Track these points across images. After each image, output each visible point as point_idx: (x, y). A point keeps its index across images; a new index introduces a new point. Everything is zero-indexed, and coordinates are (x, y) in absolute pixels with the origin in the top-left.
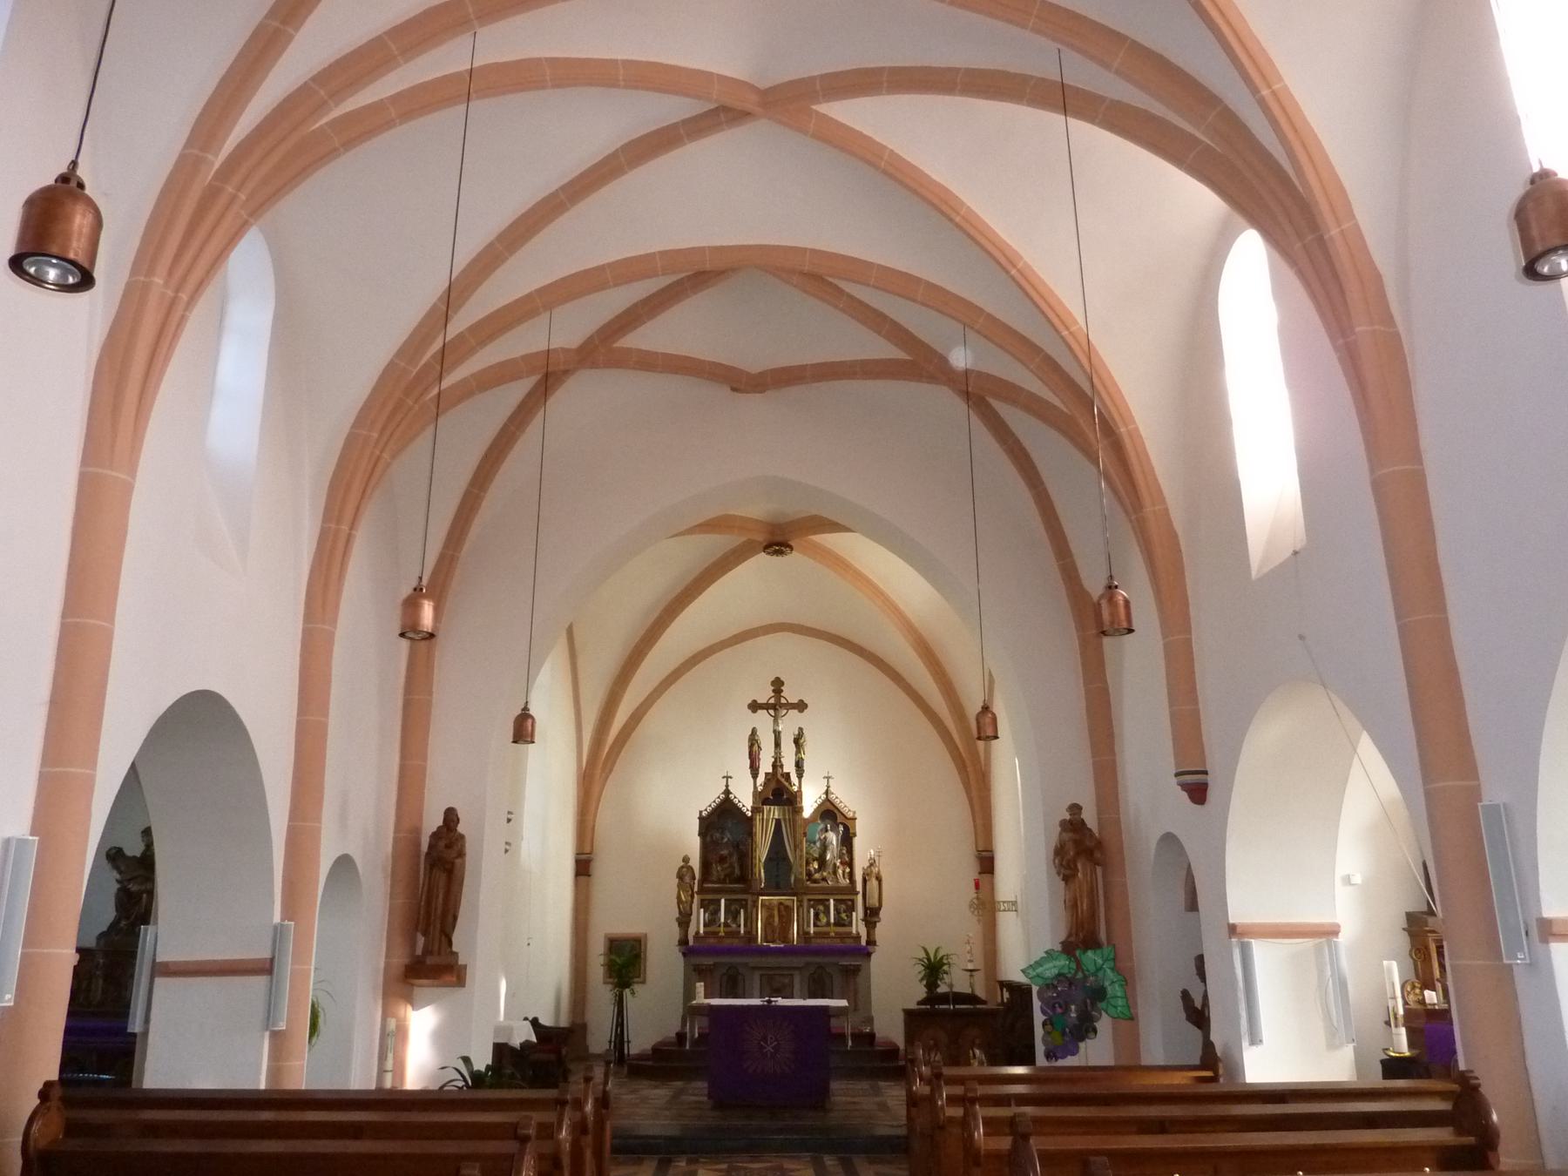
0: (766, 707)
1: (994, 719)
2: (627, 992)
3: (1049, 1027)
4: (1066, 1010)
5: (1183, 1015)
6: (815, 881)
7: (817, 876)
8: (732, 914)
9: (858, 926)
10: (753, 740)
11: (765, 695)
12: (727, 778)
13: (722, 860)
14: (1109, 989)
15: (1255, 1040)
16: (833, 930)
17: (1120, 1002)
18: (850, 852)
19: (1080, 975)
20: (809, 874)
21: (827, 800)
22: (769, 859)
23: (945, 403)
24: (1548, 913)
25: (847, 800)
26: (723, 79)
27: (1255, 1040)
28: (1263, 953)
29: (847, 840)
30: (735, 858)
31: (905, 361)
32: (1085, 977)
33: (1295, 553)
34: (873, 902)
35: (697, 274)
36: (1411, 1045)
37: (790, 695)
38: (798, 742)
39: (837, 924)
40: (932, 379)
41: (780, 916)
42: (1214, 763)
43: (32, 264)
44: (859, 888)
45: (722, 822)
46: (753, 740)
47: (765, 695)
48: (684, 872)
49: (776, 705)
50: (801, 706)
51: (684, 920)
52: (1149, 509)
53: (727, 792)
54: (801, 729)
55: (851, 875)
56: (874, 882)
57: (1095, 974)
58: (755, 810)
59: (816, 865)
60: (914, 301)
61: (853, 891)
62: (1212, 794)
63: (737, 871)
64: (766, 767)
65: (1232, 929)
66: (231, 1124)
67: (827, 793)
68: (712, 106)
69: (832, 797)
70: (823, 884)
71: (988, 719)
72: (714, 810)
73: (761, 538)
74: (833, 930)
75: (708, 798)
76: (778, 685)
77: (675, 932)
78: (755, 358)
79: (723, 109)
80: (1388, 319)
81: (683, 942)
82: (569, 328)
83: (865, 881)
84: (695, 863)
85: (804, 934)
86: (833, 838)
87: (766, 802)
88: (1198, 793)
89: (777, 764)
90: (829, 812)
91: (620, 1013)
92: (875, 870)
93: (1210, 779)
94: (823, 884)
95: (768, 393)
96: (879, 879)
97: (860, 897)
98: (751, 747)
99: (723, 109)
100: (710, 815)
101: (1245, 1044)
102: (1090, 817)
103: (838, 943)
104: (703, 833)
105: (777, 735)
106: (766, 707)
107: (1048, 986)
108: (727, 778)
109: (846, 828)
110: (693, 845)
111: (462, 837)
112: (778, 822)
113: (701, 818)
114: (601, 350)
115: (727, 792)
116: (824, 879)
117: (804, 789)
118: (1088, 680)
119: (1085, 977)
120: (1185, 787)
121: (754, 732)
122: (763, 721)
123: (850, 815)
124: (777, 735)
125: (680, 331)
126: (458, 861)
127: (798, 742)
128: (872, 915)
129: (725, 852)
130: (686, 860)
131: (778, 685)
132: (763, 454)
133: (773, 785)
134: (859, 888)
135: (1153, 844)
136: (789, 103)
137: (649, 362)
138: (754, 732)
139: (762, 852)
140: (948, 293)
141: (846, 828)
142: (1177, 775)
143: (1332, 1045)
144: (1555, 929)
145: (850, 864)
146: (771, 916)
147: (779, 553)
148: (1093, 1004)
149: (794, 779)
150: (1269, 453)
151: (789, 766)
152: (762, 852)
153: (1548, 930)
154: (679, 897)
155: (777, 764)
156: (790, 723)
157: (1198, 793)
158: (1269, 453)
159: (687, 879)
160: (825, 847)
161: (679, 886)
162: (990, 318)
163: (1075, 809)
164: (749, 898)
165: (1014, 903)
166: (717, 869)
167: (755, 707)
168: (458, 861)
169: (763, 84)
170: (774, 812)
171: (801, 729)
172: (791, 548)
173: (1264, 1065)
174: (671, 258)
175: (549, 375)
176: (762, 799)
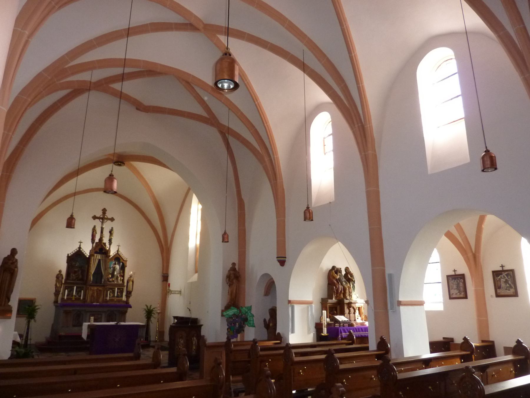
0: (99, 218)
1: (228, 236)
2: (32, 321)
3: (229, 330)
4: (235, 325)
5: (263, 325)
6: (110, 282)
7: (111, 280)
8: (78, 292)
9: (124, 298)
10: (94, 230)
11: (99, 214)
12: (81, 242)
13: (75, 272)
14: (249, 319)
15: (293, 332)
16: (116, 299)
17: (252, 322)
18: (124, 272)
19: (240, 314)
20: (108, 279)
21: (118, 253)
22: (94, 273)
23: (213, 133)
24: (400, 300)
25: (125, 254)
26: (196, 17)
27: (293, 332)
28: (297, 308)
29: (123, 268)
30: (80, 272)
31: (206, 118)
32: (242, 315)
33: (330, 203)
34: (130, 289)
35: (150, 71)
36: (327, 333)
37: (109, 215)
38: (111, 232)
39: (117, 297)
40: (212, 125)
41: (97, 294)
42: (289, 254)
43: (220, 83)
44: (125, 284)
45: (76, 259)
46: (94, 230)
47: (99, 214)
48: (59, 276)
49: (103, 219)
50: (112, 220)
51: (57, 294)
52: (278, 181)
53: (80, 248)
54: (112, 228)
55: (123, 280)
56: (131, 283)
57: (245, 314)
58: (91, 255)
59: (110, 276)
60: (221, 101)
61: (123, 285)
62: (286, 263)
63: (80, 277)
64: (97, 240)
65: (289, 302)
66: (122, 367)
67: (118, 251)
68: (187, 22)
69: (119, 253)
70: (113, 283)
71: (226, 236)
72: (74, 254)
73: (115, 159)
74: (116, 299)
75: (72, 249)
76: (104, 211)
77: (53, 298)
78: (147, 102)
79: (190, 25)
80: (375, 151)
81: (56, 302)
82: (98, 75)
83: (128, 282)
84: (64, 273)
85: (63, 299)
86: (117, 267)
87: (96, 253)
88: (282, 263)
89: (101, 240)
90: (118, 258)
91: (28, 329)
92: (132, 279)
93: (287, 259)
94: (113, 283)
95: (149, 113)
96: (133, 282)
97: (125, 288)
98: (93, 232)
99: (190, 25)
100: (72, 255)
101: (290, 333)
102: (237, 267)
103: (118, 304)
104: (68, 262)
105: (102, 229)
106: (99, 218)
107: (230, 318)
108: (81, 242)
109: (123, 264)
110: (63, 266)
111: (16, 260)
112: (99, 260)
113: (68, 257)
114: (102, 86)
115: (80, 248)
116: (113, 281)
117: (111, 249)
118: (239, 226)
119: (242, 315)
120: (279, 261)
121: (95, 227)
122: (98, 223)
123: (125, 259)
124: (102, 229)
125: (129, 88)
126: (16, 269)
127: (111, 232)
128: (129, 294)
129: (76, 270)
130: (60, 271)
131: (104, 211)
132: (136, 133)
133: (100, 247)
134: (125, 284)
135: (259, 277)
136: (210, 30)
137: (121, 96)
138: (95, 227)
139: (93, 270)
140: (232, 102)
141: (123, 263)
142: (277, 257)
143: (309, 333)
144: (402, 303)
145: (123, 276)
146: (94, 293)
147: (120, 165)
148: (244, 324)
149: (107, 245)
150: (322, 173)
151: (106, 240)
152: (93, 270)
153: (400, 303)
154: (56, 285)
155: (101, 240)
156: (108, 226)
157: (282, 263)
158: (322, 173)
159: (60, 279)
160: (114, 269)
161: (56, 281)
162: (242, 113)
163: (234, 264)
164: (84, 286)
165: (180, 292)
166: (73, 276)
167: (95, 218)
168: (16, 269)
169: (205, 22)
170: (99, 257)
171: (112, 228)
172: (124, 164)
173: (294, 339)
174: (135, 62)
175: (211, 120)
176: (94, 251)
